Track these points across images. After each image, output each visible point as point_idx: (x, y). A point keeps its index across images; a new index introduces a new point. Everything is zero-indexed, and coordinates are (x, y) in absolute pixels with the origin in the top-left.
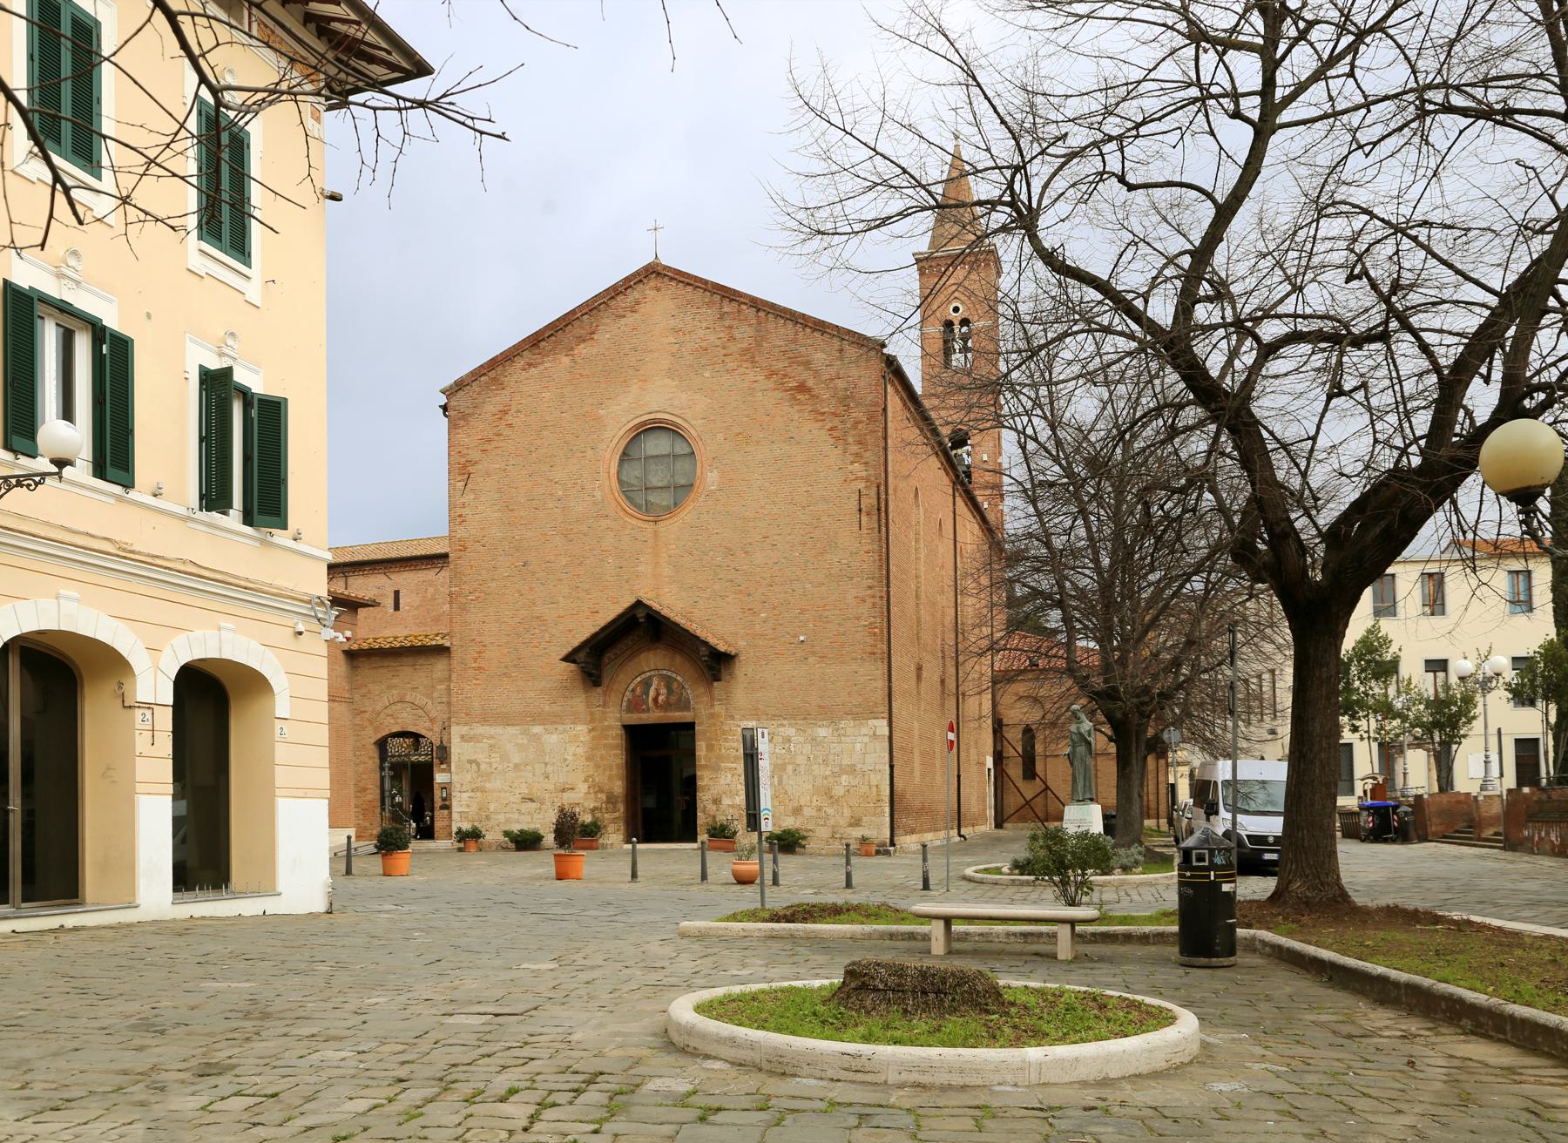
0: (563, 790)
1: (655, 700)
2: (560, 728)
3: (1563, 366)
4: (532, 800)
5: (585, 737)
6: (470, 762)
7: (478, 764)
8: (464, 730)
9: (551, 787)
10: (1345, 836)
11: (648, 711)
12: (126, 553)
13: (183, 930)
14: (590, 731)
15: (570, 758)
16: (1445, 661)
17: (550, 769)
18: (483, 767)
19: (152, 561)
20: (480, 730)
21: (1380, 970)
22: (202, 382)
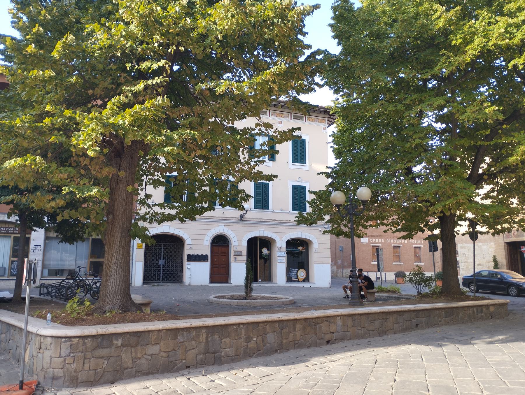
0: (489, 262)
1: (514, 234)
2: (487, 244)
3: (2, 358)
4: (480, 265)
5: (494, 246)
6: (463, 254)
7: (465, 255)
8: (461, 245)
9: (485, 261)
10: (207, 256)
11: (512, 237)
12: (274, 221)
13: (182, 255)
14: (495, 244)
15: (490, 252)
16: (295, 188)
17: (485, 256)
18: (467, 255)
19: (280, 222)
20: (465, 245)
21: (263, 295)
22: (293, 188)
